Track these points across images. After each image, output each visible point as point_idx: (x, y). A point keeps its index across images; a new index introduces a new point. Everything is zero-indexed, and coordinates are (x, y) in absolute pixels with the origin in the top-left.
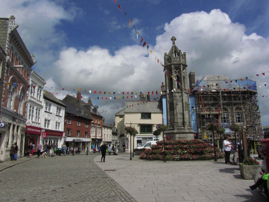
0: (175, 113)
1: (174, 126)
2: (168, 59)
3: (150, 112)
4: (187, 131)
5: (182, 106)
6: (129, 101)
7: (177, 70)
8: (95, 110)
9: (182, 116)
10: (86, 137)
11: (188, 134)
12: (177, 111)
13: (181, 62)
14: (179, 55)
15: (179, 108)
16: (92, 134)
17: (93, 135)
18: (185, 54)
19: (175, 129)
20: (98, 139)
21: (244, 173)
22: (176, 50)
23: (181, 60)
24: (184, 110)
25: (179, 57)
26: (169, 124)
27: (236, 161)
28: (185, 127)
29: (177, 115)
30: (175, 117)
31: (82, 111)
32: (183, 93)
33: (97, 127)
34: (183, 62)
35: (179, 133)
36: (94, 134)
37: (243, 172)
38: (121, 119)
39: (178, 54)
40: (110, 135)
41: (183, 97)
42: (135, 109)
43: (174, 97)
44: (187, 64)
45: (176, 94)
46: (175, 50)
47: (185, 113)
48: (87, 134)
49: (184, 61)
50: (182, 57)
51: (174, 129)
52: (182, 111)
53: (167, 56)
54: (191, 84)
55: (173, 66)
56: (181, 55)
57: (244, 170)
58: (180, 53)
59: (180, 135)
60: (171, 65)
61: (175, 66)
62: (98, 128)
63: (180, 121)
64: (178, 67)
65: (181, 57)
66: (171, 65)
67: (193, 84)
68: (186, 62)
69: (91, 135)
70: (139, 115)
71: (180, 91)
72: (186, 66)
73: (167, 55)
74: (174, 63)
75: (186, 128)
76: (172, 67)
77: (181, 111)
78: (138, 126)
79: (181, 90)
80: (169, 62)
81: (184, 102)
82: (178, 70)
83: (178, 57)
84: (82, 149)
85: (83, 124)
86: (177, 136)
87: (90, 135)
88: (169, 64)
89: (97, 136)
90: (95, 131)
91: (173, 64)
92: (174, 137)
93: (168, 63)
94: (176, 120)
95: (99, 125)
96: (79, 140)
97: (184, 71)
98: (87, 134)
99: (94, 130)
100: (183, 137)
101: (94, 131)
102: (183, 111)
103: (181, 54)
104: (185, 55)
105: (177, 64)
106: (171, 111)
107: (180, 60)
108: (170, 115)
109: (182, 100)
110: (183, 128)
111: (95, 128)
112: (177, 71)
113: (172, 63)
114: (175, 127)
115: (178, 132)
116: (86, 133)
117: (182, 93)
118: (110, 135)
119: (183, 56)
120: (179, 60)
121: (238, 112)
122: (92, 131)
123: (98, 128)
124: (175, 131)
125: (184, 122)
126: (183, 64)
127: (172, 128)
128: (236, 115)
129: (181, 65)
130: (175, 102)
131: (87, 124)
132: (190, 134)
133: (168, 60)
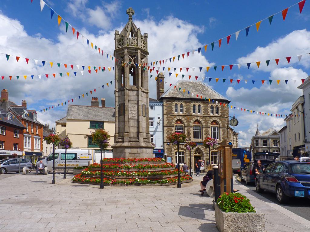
0: (126, 119)
1: (124, 136)
2: (120, 40)
3: (102, 120)
4: (143, 145)
5: (136, 109)
6: (75, 105)
7: (132, 58)
8: (31, 115)
9: (136, 123)
10: (15, 149)
11: (144, 149)
12: (130, 116)
13: (140, 47)
14: (136, 35)
15: (132, 113)
16: (36, 147)
17: (27, 148)
18: (146, 35)
19: (125, 142)
20: (37, 154)
21: (225, 228)
22: (133, 29)
23: (140, 43)
24: (140, 115)
25: (136, 38)
26: (116, 134)
27: (209, 190)
28: (140, 138)
29: (129, 121)
30: (127, 124)
31: (8, 115)
32: (140, 91)
33: (34, 138)
34: (143, 47)
35: (131, 147)
36: (29, 146)
37: (224, 226)
38: (63, 129)
39: (136, 34)
40: (51, 148)
41: (140, 96)
42: (81, 117)
43: (126, 97)
44: (149, 51)
45: (130, 91)
46: (131, 28)
47: (140, 120)
48: (18, 145)
49: (143, 45)
50: (142, 38)
51: (123, 142)
52: (136, 117)
53: (118, 36)
54: (159, 89)
55: (126, 51)
56: (139, 36)
57: (226, 222)
58: (138, 32)
59: (132, 149)
60: (123, 49)
61: (130, 51)
62: (36, 139)
63: (133, 131)
64: (133, 52)
65: (140, 40)
66: (123, 49)
67: (161, 89)
68: (147, 48)
69: (24, 147)
70: (88, 124)
71: (136, 88)
72: (147, 53)
73: (119, 35)
74: (128, 46)
75: (141, 141)
76: (125, 52)
77: (135, 116)
78: (85, 138)
79: (138, 87)
80: (121, 44)
81: (140, 104)
82: (134, 58)
83: (135, 38)
84: (302, 159)
85: (8, 132)
86: (128, 151)
87: (23, 147)
88: (121, 47)
89: (35, 148)
90: (30, 142)
91: (126, 47)
92: (123, 152)
93: (119, 46)
94: (127, 129)
95: (37, 135)
96: (3, 154)
97: (143, 60)
98: (18, 145)
99: (38, 142)
100: (136, 152)
101: (38, 144)
102: (138, 116)
103: (139, 33)
104: (146, 37)
105: (132, 48)
106: (121, 116)
107: (137, 43)
108: (118, 122)
109: (138, 101)
110: (137, 140)
111: (40, 140)
112: (133, 59)
113: (125, 46)
114: (126, 139)
115: (130, 145)
116: (15, 144)
117: (138, 91)
118: (51, 148)
119: (143, 37)
120: (136, 43)
121: (213, 127)
122: (36, 144)
123: (36, 139)
124: (126, 144)
125: (139, 133)
126: (142, 49)
127: (120, 140)
128: (211, 130)
129: (139, 51)
130: (126, 103)
131: (19, 133)
132: (147, 149)
133: (119, 42)
